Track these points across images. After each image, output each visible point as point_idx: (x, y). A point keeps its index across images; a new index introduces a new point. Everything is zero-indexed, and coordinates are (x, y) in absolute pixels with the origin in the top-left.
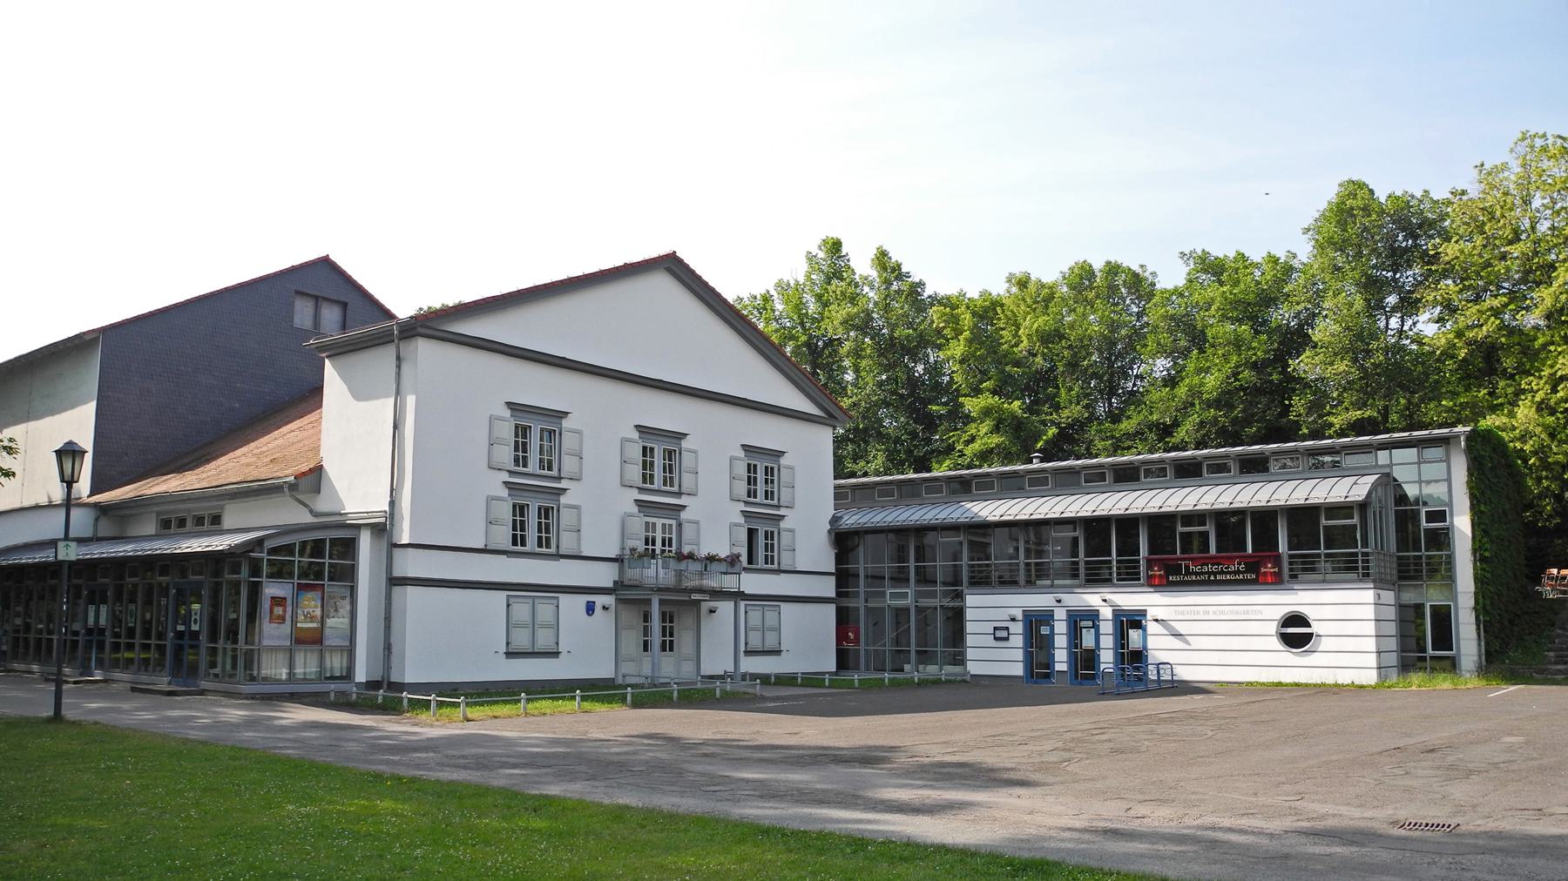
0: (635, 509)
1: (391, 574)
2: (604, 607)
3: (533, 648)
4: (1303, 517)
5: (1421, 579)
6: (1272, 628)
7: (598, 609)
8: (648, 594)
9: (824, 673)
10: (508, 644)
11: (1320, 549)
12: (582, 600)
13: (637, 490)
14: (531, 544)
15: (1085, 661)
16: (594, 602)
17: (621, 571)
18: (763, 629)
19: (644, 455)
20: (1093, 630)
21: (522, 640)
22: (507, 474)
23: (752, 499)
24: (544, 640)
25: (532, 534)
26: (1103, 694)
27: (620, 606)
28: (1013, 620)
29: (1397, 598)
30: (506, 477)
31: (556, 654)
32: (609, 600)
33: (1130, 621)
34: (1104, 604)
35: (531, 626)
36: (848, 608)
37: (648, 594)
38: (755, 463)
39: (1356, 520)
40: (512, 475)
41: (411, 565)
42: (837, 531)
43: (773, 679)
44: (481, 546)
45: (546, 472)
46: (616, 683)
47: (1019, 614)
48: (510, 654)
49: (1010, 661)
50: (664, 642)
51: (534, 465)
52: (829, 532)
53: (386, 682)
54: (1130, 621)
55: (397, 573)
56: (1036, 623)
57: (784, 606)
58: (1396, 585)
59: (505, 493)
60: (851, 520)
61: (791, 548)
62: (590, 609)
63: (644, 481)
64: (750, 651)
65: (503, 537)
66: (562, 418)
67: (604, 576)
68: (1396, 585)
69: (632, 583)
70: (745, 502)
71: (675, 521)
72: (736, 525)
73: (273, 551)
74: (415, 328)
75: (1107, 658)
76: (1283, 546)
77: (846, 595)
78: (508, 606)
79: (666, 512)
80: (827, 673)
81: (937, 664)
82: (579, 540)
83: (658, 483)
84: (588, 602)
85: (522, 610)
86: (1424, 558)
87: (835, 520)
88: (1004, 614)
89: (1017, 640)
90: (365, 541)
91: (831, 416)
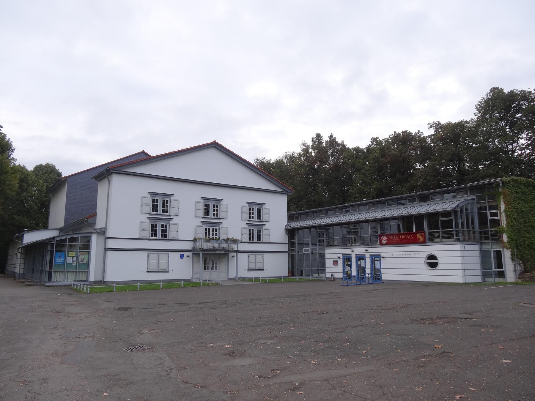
0: (201, 224)
1: (106, 247)
3: (158, 269)
4: (432, 217)
5: (489, 240)
6: (423, 260)
7: (185, 256)
8: (199, 252)
9: (281, 277)
10: (248, 267)
11: (439, 229)
13: (202, 218)
14: (255, 240)
15: (361, 270)
19: (250, 210)
20: (379, 261)
21: (252, 266)
22: (149, 215)
24: (259, 266)
26: (343, 285)
27: (194, 255)
28: (339, 258)
29: (481, 247)
31: (263, 270)
32: (190, 254)
33: (374, 258)
34: (366, 252)
37: (199, 252)
39: (453, 218)
40: (150, 215)
41: (111, 244)
43: (253, 280)
47: (341, 256)
48: (248, 270)
49: (338, 272)
53: (103, 281)
54: (374, 258)
56: (347, 258)
57: (265, 255)
58: (479, 243)
59: (247, 226)
60: (295, 225)
61: (268, 235)
62: (182, 257)
64: (249, 270)
66: (263, 205)
67: (189, 246)
68: (479, 243)
69: (197, 248)
71: (218, 227)
73: (57, 241)
74: (110, 171)
75: (368, 271)
76: (426, 229)
78: (248, 257)
79: (212, 225)
80: (267, 277)
81: (317, 274)
83: (211, 215)
84: (181, 254)
85: (154, 257)
86: (489, 231)
87: (287, 225)
88: (335, 256)
89: (341, 265)
90: (94, 239)
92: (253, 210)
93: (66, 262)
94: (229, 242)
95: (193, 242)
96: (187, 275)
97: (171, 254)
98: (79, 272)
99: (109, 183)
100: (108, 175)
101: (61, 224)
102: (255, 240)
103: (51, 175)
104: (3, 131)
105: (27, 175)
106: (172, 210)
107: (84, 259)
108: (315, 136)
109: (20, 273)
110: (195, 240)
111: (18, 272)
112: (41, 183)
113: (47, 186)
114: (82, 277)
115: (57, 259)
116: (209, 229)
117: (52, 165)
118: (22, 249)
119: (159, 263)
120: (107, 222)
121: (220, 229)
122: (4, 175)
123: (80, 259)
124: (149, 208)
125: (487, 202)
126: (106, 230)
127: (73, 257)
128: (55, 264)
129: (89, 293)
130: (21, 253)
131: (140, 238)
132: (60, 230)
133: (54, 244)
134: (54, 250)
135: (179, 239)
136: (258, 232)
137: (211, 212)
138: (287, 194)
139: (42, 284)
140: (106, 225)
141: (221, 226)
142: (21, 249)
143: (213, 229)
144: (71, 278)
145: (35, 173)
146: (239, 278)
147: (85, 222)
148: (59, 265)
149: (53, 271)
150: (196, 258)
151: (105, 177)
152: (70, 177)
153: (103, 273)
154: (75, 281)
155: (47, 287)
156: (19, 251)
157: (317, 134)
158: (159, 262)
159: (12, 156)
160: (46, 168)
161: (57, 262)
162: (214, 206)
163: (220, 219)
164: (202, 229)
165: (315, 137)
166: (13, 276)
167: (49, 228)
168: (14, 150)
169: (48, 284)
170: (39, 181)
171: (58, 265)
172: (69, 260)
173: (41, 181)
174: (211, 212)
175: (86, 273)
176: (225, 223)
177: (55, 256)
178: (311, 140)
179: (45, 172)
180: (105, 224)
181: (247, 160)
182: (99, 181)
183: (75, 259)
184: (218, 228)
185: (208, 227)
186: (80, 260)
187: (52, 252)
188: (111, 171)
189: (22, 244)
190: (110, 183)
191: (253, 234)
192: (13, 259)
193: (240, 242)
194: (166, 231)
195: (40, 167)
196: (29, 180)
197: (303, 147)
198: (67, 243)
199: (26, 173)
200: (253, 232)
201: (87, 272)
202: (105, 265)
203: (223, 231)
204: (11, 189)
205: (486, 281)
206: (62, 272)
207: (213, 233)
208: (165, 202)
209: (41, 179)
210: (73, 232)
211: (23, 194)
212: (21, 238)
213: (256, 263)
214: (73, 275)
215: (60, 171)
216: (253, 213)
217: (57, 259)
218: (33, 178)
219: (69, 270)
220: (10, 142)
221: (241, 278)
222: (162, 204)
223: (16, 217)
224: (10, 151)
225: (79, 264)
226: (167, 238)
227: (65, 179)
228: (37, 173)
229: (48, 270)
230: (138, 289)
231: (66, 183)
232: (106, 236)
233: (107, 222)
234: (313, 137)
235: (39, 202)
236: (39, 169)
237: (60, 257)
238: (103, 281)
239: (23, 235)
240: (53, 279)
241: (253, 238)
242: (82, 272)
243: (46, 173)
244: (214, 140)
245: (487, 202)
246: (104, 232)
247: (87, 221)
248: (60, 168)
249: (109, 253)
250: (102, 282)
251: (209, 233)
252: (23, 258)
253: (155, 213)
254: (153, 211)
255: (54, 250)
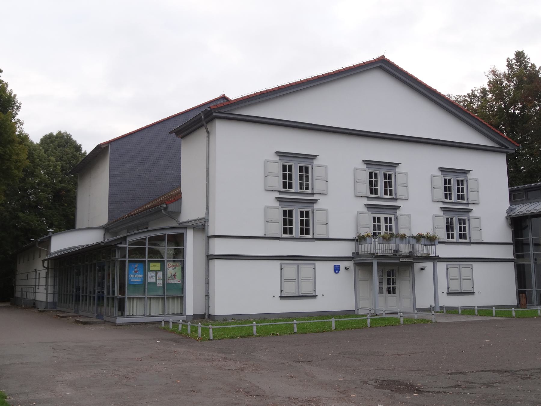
0: (366, 210)
1: (208, 253)
2: (346, 268)
7: (342, 269)
9: (492, 307)
10: (448, 288)
12: (332, 264)
13: (366, 199)
14: (456, 239)
16: (339, 265)
17: (357, 248)
18: (460, 279)
19: (445, 183)
21: (291, 289)
22: (442, 203)
23: (448, 200)
25: (456, 232)
27: (357, 268)
30: (278, 195)
31: (315, 297)
35: (297, 281)
36: (524, 265)
38: (450, 178)
42: (511, 217)
43: (476, 311)
44: (263, 235)
45: (304, 191)
46: (356, 313)
48: (282, 297)
50: (389, 288)
51: (454, 198)
52: (507, 218)
53: (207, 315)
55: (211, 253)
57: (475, 265)
59: (441, 213)
60: (522, 209)
62: (337, 269)
63: (446, 198)
65: (277, 229)
67: (347, 250)
69: (362, 253)
70: (443, 202)
71: (394, 215)
72: (437, 216)
74: (212, 113)
77: (522, 256)
82: (327, 229)
83: (381, 192)
84: (335, 265)
85: (290, 270)
87: (510, 210)
90: (190, 237)
91: (504, 146)
92: (450, 183)
93: (146, 281)
94: (423, 241)
95: (353, 244)
96: (348, 305)
97: (318, 264)
98: (150, 298)
99: (208, 137)
100: (207, 123)
101: (104, 220)
102: (456, 239)
103: (67, 150)
104: (4, 78)
105: (32, 150)
106: (317, 186)
107: (174, 275)
108: (512, 57)
109: (49, 301)
110: (360, 239)
111: (44, 300)
112: (53, 162)
113: (62, 167)
114: (173, 307)
115: (131, 276)
116: (379, 219)
117: (66, 134)
118: (49, 261)
119: (297, 279)
120: (207, 207)
121: (397, 218)
122: (9, 146)
123: (169, 274)
124: (277, 182)
125: (147, 261)
126: (208, 222)
127: (157, 272)
128: (129, 285)
129: (211, 338)
130: (48, 268)
131: (266, 236)
132: (106, 229)
133: (125, 248)
134: (127, 259)
135: (483, 242)
136: (460, 223)
137: (381, 188)
138: (506, 153)
139: (105, 321)
140: (207, 213)
141: (399, 212)
142: (47, 261)
143: (386, 219)
144: (155, 308)
145: (43, 148)
146: (442, 308)
147: (163, 210)
148: (135, 286)
149: (126, 297)
150: (359, 271)
151: (202, 126)
152: (113, 143)
153: (207, 300)
154: (163, 314)
155: (118, 325)
156: (45, 266)
157: (516, 53)
158: (300, 280)
159: (17, 117)
160: (58, 139)
161: (131, 280)
162: (385, 175)
163: (396, 199)
164: (367, 219)
165: (514, 57)
166: (33, 305)
167: (77, 228)
168: (19, 107)
169: (119, 320)
170: (49, 158)
171: (135, 285)
172: (151, 278)
173: (53, 159)
174: (381, 188)
175: (179, 300)
176: (405, 208)
177: (128, 270)
178: (506, 63)
179: (57, 144)
180: (204, 211)
181: (439, 90)
182: (183, 137)
183: (160, 274)
184: (393, 217)
185: (377, 216)
186: (168, 278)
187: (123, 263)
188: (214, 114)
189: (48, 252)
190: (210, 135)
191: (452, 227)
192: (27, 279)
193: (440, 242)
194: (307, 224)
195: (50, 138)
196: (35, 157)
197: (492, 77)
198: (147, 247)
199: (32, 147)
200: (452, 223)
201: (182, 299)
202: (208, 286)
203: (402, 221)
204: (18, 168)
205: (152, 314)
206: (140, 298)
207: (386, 226)
208: (304, 170)
209: (53, 156)
210: (128, 232)
211: (28, 179)
212: (47, 243)
213: (460, 281)
214: (159, 302)
215: (78, 143)
216: (450, 188)
217: (131, 276)
218: (40, 155)
219: (152, 295)
220: (13, 95)
221: (445, 309)
222: (299, 174)
223: (20, 214)
224: (14, 110)
225: (168, 284)
226: (310, 236)
227: (106, 145)
228: (46, 147)
229: (117, 295)
230: (295, 330)
231: (108, 152)
232: (208, 232)
233: (207, 207)
234: (509, 58)
235: (51, 191)
236: (48, 140)
237: (136, 272)
238: (207, 315)
239: (50, 238)
240: (127, 313)
241: (453, 235)
242: (173, 298)
243: (59, 146)
244: (380, 56)
245: (147, 261)
246: (204, 225)
247: (166, 209)
248: (78, 139)
249: (217, 264)
250: (206, 317)
251: (379, 226)
252: (50, 277)
253: (287, 190)
254: (284, 186)
255: (127, 259)
